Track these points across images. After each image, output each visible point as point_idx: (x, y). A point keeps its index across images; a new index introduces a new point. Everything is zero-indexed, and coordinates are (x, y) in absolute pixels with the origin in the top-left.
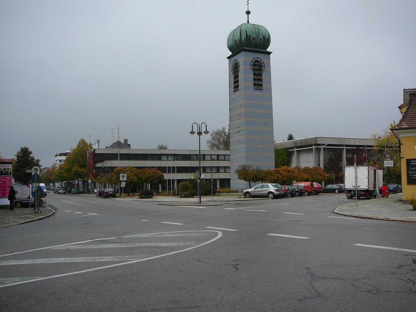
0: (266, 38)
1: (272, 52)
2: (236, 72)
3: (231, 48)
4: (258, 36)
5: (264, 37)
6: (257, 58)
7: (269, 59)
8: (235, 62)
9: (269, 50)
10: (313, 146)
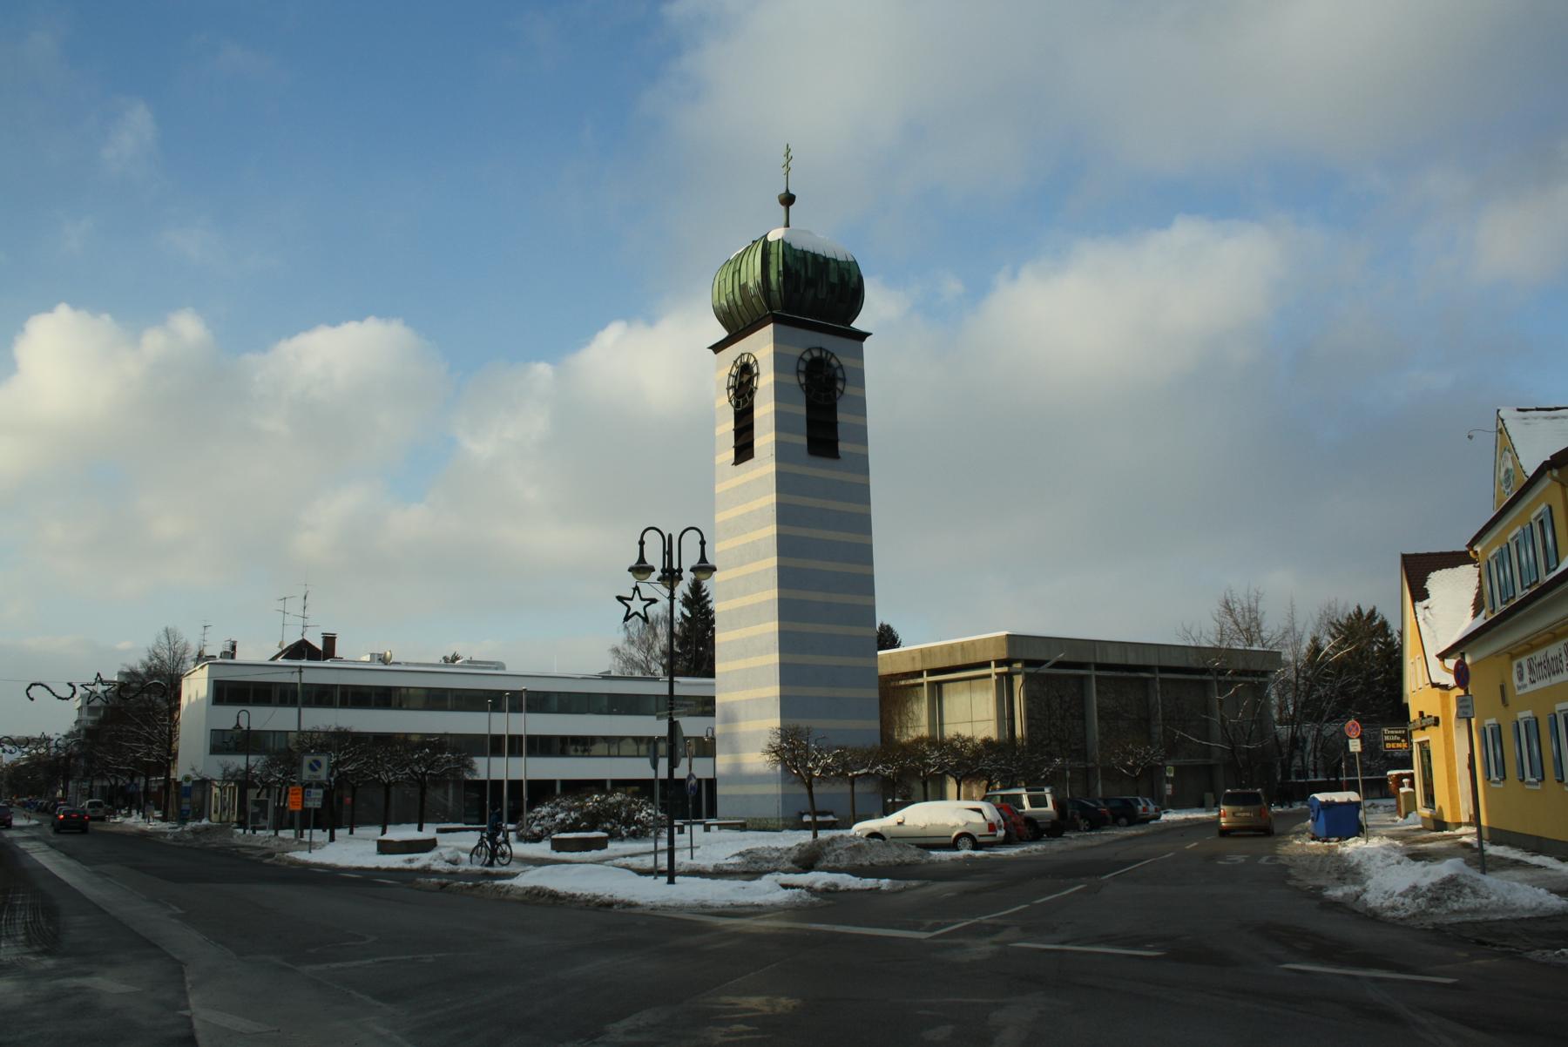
1: (870, 334)
3: (725, 317)
5: (841, 277)
6: (821, 349)
7: (859, 355)
8: (738, 362)
9: (858, 324)
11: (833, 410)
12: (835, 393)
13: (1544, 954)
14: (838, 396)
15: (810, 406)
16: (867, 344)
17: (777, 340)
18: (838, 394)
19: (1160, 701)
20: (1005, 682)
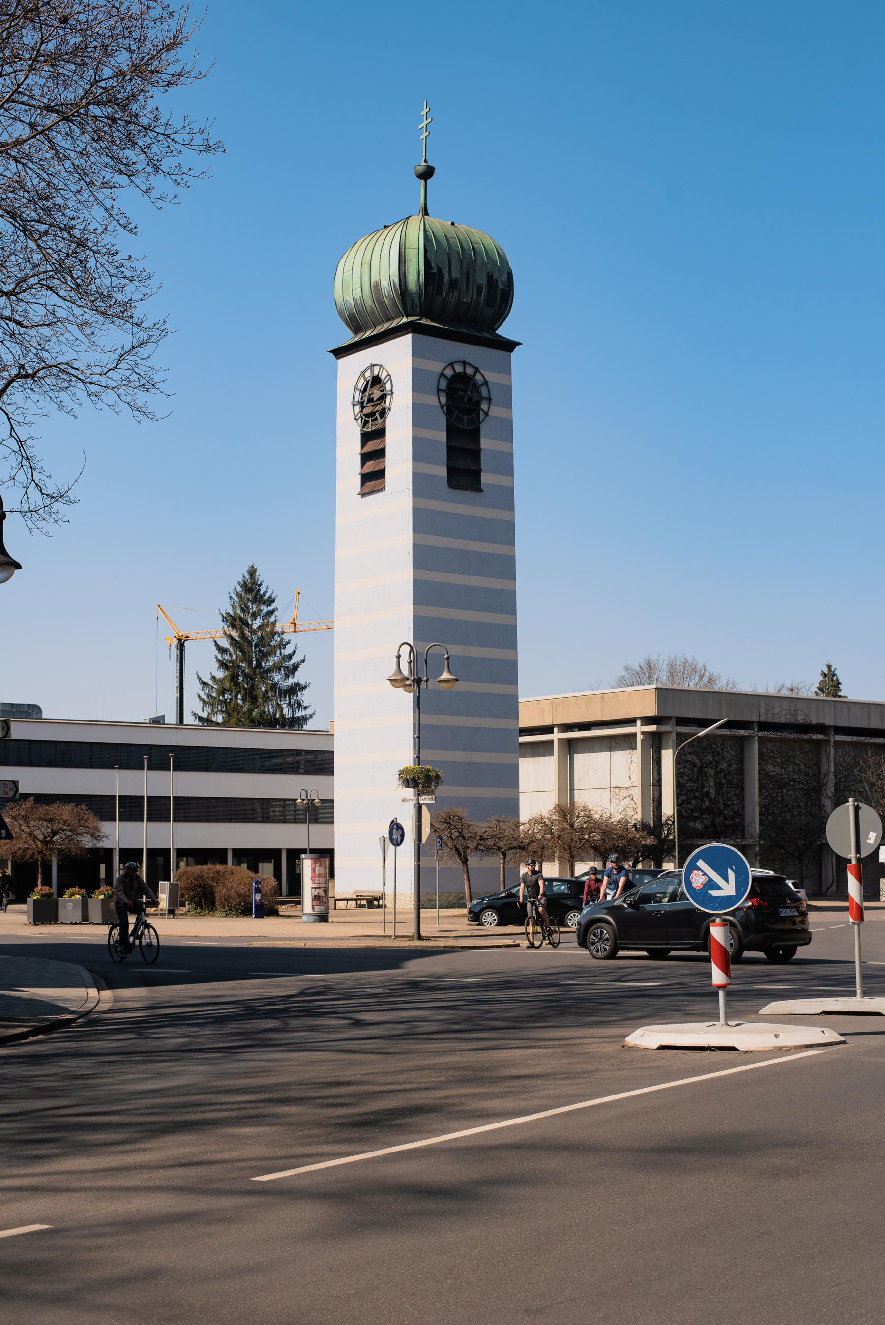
0: (500, 286)
2: (372, 415)
4: (468, 273)
5: (490, 277)
6: (464, 363)
9: (505, 331)
10: (552, 732)
11: (475, 434)
12: (478, 416)
13: (514, 942)
14: (481, 418)
15: (451, 431)
16: (516, 355)
17: (417, 352)
18: (482, 416)
19: (832, 769)
20: (655, 742)
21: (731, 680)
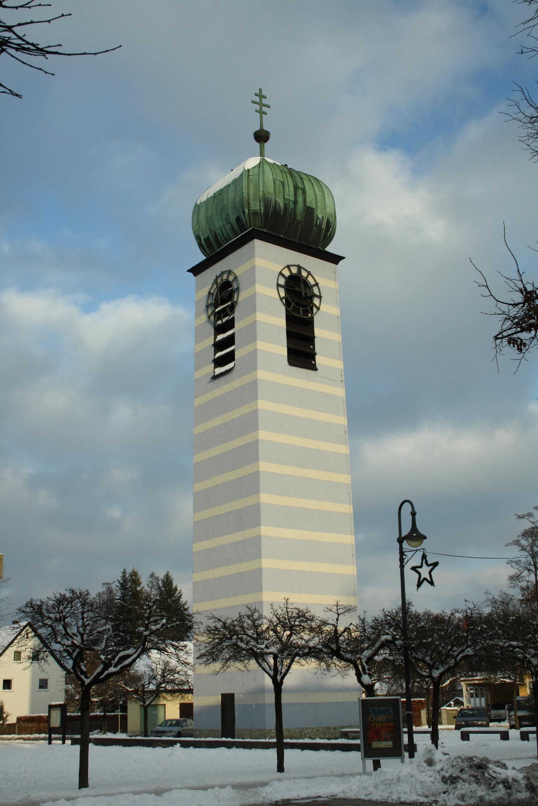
1: (345, 258)
11: (310, 324)
15: (290, 319)
21: (509, 586)
